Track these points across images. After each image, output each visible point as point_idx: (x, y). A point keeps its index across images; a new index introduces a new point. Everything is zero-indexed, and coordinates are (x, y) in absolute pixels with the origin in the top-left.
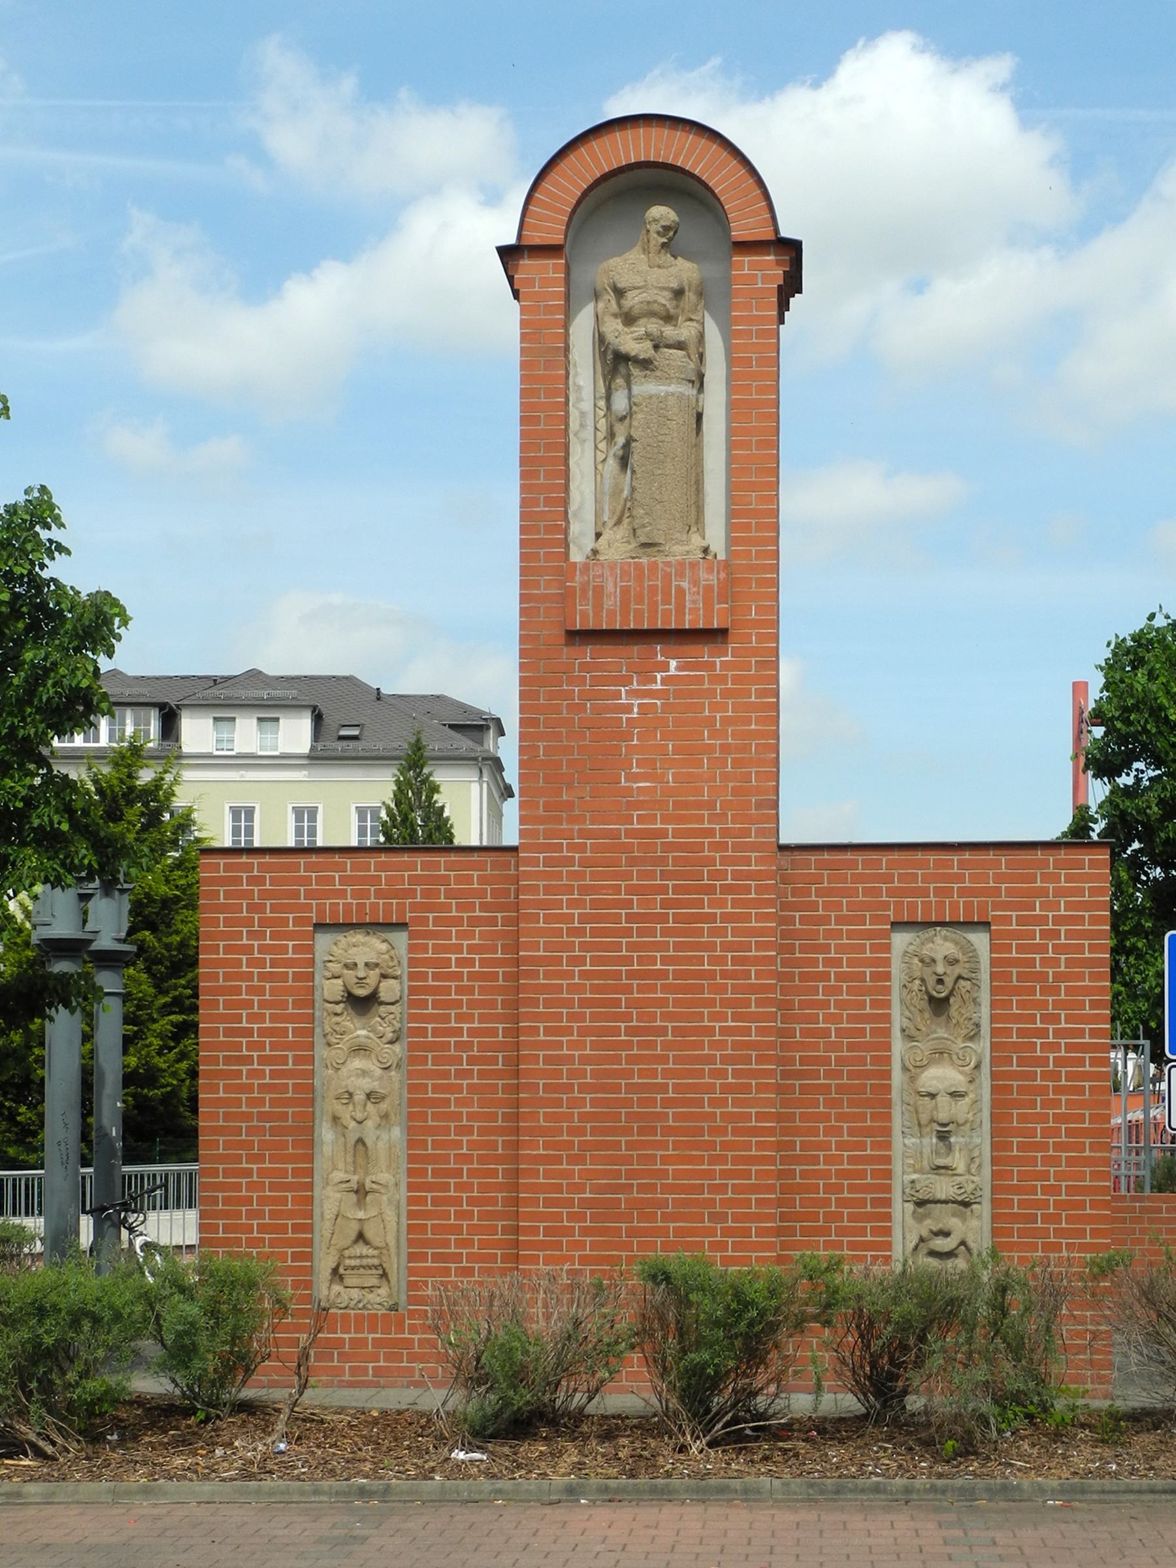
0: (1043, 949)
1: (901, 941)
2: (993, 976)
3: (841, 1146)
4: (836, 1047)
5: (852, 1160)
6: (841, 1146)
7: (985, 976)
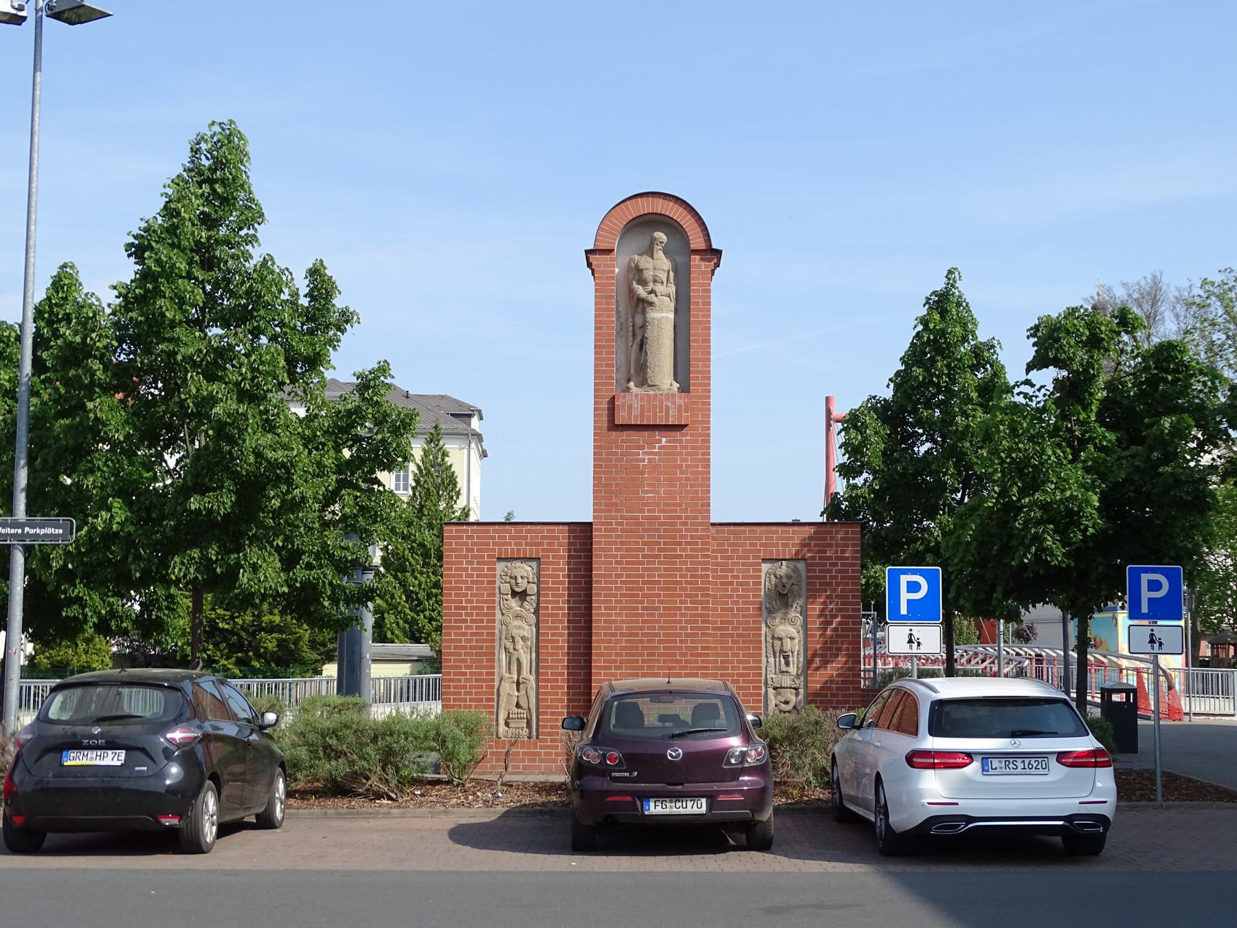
0: (830, 571)
1: (765, 567)
2: (808, 584)
3: (739, 662)
4: (736, 616)
5: (744, 668)
6: (739, 662)
7: (804, 584)
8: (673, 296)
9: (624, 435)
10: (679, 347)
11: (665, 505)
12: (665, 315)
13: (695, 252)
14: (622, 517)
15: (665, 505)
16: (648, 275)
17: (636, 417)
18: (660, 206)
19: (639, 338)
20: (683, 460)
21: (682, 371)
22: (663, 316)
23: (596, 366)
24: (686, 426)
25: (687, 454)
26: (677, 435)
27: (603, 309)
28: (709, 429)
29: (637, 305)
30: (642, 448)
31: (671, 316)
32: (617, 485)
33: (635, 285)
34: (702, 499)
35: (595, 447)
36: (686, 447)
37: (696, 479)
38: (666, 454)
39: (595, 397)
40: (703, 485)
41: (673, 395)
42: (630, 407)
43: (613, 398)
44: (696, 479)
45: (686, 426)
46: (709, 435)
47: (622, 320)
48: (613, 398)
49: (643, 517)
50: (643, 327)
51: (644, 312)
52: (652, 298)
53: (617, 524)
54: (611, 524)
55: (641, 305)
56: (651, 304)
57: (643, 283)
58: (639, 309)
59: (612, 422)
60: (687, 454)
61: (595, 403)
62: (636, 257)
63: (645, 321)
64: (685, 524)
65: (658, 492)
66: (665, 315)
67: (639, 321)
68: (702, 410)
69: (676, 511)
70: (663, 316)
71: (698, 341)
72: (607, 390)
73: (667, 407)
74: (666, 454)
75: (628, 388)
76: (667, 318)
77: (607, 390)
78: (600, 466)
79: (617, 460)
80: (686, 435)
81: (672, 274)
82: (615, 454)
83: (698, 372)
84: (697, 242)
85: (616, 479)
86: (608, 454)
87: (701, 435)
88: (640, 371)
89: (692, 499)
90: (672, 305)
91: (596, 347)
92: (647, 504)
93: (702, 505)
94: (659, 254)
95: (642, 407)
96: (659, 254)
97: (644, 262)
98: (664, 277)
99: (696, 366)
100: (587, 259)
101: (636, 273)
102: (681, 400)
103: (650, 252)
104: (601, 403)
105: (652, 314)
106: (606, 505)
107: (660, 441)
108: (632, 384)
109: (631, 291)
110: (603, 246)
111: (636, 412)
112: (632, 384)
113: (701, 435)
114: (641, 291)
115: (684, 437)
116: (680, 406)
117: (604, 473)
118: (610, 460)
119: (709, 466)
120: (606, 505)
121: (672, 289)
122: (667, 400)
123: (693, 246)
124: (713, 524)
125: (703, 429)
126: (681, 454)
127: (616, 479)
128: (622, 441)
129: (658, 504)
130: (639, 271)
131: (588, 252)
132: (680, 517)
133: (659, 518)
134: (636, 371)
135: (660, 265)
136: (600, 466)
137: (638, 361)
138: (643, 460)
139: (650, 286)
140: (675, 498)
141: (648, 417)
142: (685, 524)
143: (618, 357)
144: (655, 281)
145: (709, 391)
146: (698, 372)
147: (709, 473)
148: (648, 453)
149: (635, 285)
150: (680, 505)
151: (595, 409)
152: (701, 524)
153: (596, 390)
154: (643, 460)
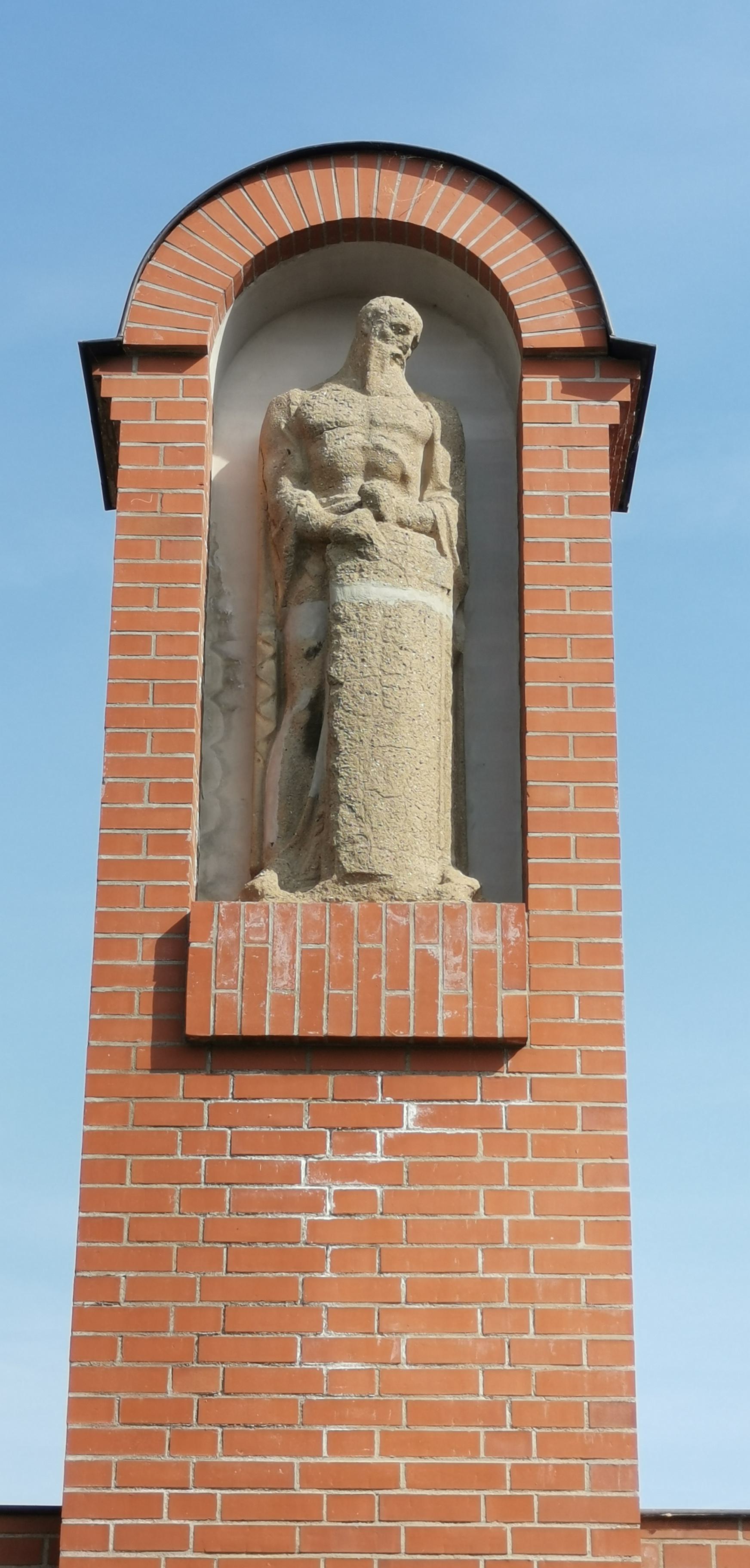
8: (450, 533)
9: (228, 1087)
10: (473, 756)
11: (417, 1413)
12: (412, 594)
13: (543, 358)
14: (208, 1475)
15: (417, 1413)
16: (345, 446)
17: (283, 1004)
18: (394, 196)
19: (302, 697)
20: (500, 1202)
21: (494, 832)
22: (404, 603)
23: (111, 793)
24: (509, 1047)
25: (520, 1174)
26: (474, 1089)
27: (148, 573)
28: (618, 1062)
29: (298, 569)
30: (309, 1145)
31: (443, 606)
32: (185, 1318)
33: (288, 487)
34: (598, 1385)
35: (90, 1142)
36: (516, 1145)
37: (565, 1291)
38: (419, 1174)
39: (102, 922)
40: (600, 1322)
41: (454, 913)
42: (257, 961)
43: (183, 928)
44: (565, 1291)
45: (509, 1047)
46: (619, 1090)
47: (233, 648)
48: (183, 928)
49: (310, 1476)
50: (322, 649)
51: (325, 586)
52: (362, 522)
53: (184, 1506)
54: (151, 1506)
55: (311, 558)
56: (357, 546)
57: (324, 477)
58: (307, 583)
59: (180, 1036)
60: (520, 1174)
61: (101, 948)
62: (297, 395)
63: (330, 620)
64: (515, 1508)
65: (381, 1354)
66: (412, 594)
67: (303, 626)
68: (588, 1034)
69: (469, 1444)
70: (404, 603)
71: (559, 697)
72: (155, 896)
73: (427, 963)
74: (419, 1174)
75: (252, 895)
76: (425, 613)
77: (155, 896)
78: (111, 1229)
79: (191, 1200)
80: (514, 1089)
81: (443, 457)
82: (184, 1173)
83: (563, 822)
84: (548, 317)
85: (181, 1290)
86: (148, 1173)
87: (582, 1090)
88: (305, 829)
89: (546, 1384)
90: (446, 569)
91: (112, 718)
92: (330, 1411)
93: (598, 1415)
94: (390, 377)
95: (312, 961)
96: (390, 377)
97: (329, 403)
98: (412, 460)
99: (551, 795)
100: (92, 385)
101: (302, 447)
102: (491, 931)
103: (357, 375)
104: (129, 949)
105: (360, 589)
106: (129, 1413)
107: (394, 1118)
108: (268, 880)
109: (268, 488)
110: (158, 334)
111: (283, 980)
112: (268, 880)
113: (582, 1090)
114: (311, 507)
115: (506, 1098)
116: (485, 959)
117: (125, 1260)
118: (158, 1202)
119: (623, 1233)
120: (129, 1413)
121: (446, 508)
122: (428, 930)
123: (532, 337)
124: (654, 1521)
125: (592, 1061)
126: (492, 1173)
127: (181, 1290)
128: (218, 1115)
129: (382, 1411)
130: (307, 433)
131: (99, 356)
132: (490, 1476)
133: (384, 1477)
134: (288, 828)
135: (388, 411)
136: (111, 1229)
137: (296, 789)
138: (314, 1203)
139: (354, 485)
140: (464, 1383)
141: (341, 1007)
142: (515, 1508)
143: (202, 790)
144: (373, 470)
145: (614, 900)
146: (563, 822)
147: (625, 1262)
148: (332, 1171)
149: (288, 487)
150: (490, 1414)
151: (99, 975)
152: (593, 1510)
153: (104, 895)
154: (314, 1203)
